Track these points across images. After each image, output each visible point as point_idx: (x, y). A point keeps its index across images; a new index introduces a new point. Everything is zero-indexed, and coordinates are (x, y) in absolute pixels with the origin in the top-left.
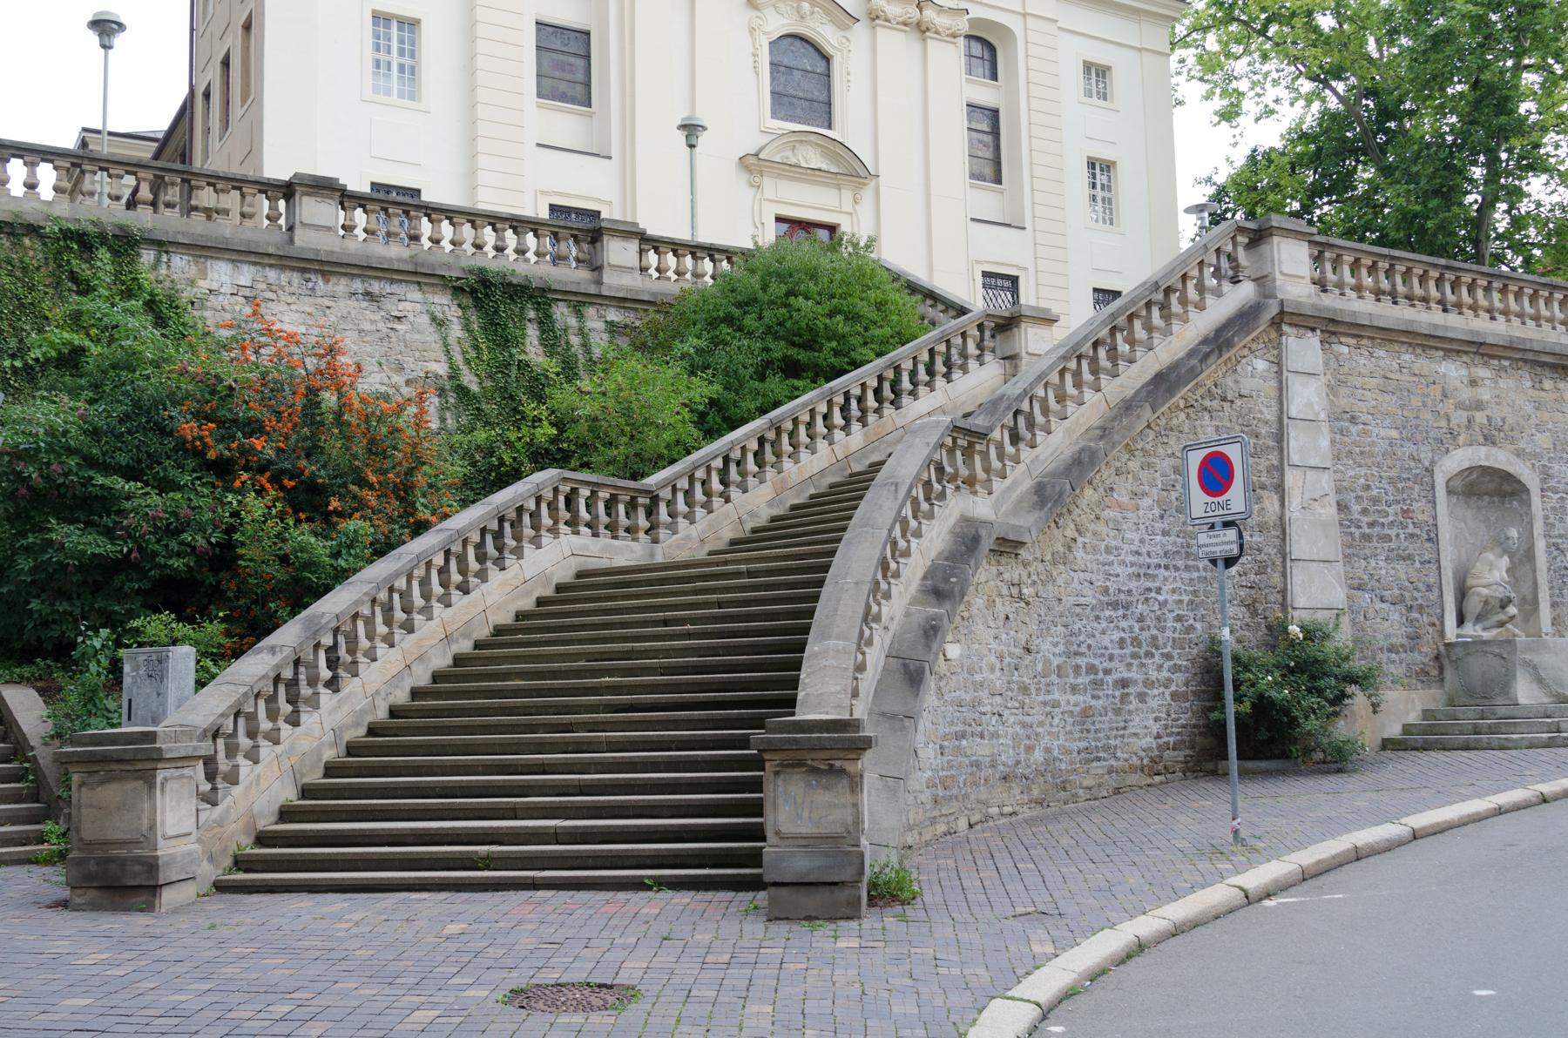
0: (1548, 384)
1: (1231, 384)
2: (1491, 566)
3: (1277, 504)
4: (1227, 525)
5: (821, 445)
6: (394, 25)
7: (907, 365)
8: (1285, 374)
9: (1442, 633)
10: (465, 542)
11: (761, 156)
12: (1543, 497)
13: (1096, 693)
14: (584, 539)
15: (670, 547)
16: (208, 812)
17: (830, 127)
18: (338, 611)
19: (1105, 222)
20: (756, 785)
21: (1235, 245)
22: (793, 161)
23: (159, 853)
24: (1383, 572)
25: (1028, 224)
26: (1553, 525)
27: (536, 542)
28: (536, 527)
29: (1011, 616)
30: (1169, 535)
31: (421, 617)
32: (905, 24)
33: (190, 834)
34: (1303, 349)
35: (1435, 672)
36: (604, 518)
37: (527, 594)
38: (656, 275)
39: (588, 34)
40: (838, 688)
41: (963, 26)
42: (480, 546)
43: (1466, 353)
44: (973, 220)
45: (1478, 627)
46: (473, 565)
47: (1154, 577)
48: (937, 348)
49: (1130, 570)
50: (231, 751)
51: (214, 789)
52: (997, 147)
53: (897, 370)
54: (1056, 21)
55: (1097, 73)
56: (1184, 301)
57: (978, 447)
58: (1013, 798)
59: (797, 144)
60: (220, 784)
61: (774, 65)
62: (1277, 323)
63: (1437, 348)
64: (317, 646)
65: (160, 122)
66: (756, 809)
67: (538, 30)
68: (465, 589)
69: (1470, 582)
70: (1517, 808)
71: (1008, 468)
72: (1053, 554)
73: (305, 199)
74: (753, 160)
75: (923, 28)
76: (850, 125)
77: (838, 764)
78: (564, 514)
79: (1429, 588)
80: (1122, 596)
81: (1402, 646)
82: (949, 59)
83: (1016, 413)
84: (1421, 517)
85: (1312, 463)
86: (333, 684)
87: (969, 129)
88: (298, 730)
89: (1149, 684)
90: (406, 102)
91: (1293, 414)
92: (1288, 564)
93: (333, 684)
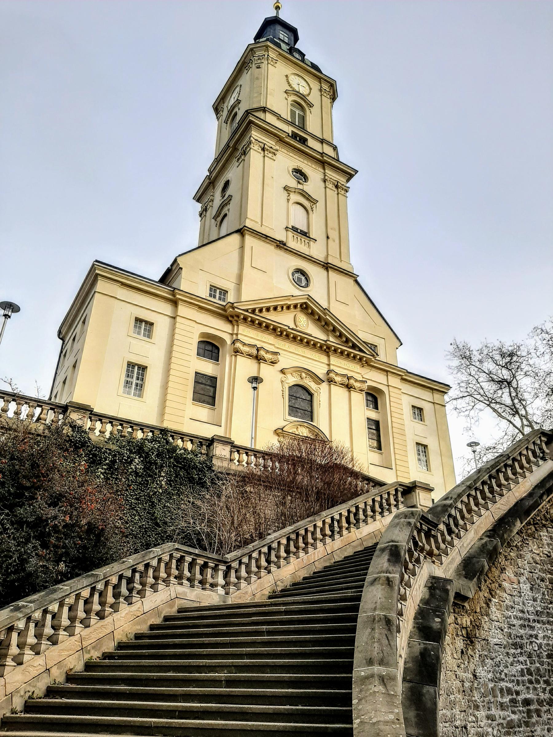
5: (319, 544)
6: (136, 368)
7: (362, 506)
13: (513, 709)
15: (235, 598)
17: (312, 421)
21: (541, 441)
22: (297, 433)
25: (394, 467)
30: (537, 601)
31: (65, 633)
36: (198, 576)
37: (145, 621)
38: (237, 463)
39: (216, 378)
40: (391, 717)
41: (365, 387)
42: (116, 587)
46: (110, 599)
47: (532, 628)
48: (376, 499)
49: (521, 622)
52: (379, 436)
53: (357, 508)
54: (401, 389)
59: (299, 426)
61: (290, 395)
67: (196, 375)
68: (101, 615)
71: (449, 549)
74: (280, 431)
78: (175, 572)
82: (359, 399)
87: (368, 428)
90: (136, 398)
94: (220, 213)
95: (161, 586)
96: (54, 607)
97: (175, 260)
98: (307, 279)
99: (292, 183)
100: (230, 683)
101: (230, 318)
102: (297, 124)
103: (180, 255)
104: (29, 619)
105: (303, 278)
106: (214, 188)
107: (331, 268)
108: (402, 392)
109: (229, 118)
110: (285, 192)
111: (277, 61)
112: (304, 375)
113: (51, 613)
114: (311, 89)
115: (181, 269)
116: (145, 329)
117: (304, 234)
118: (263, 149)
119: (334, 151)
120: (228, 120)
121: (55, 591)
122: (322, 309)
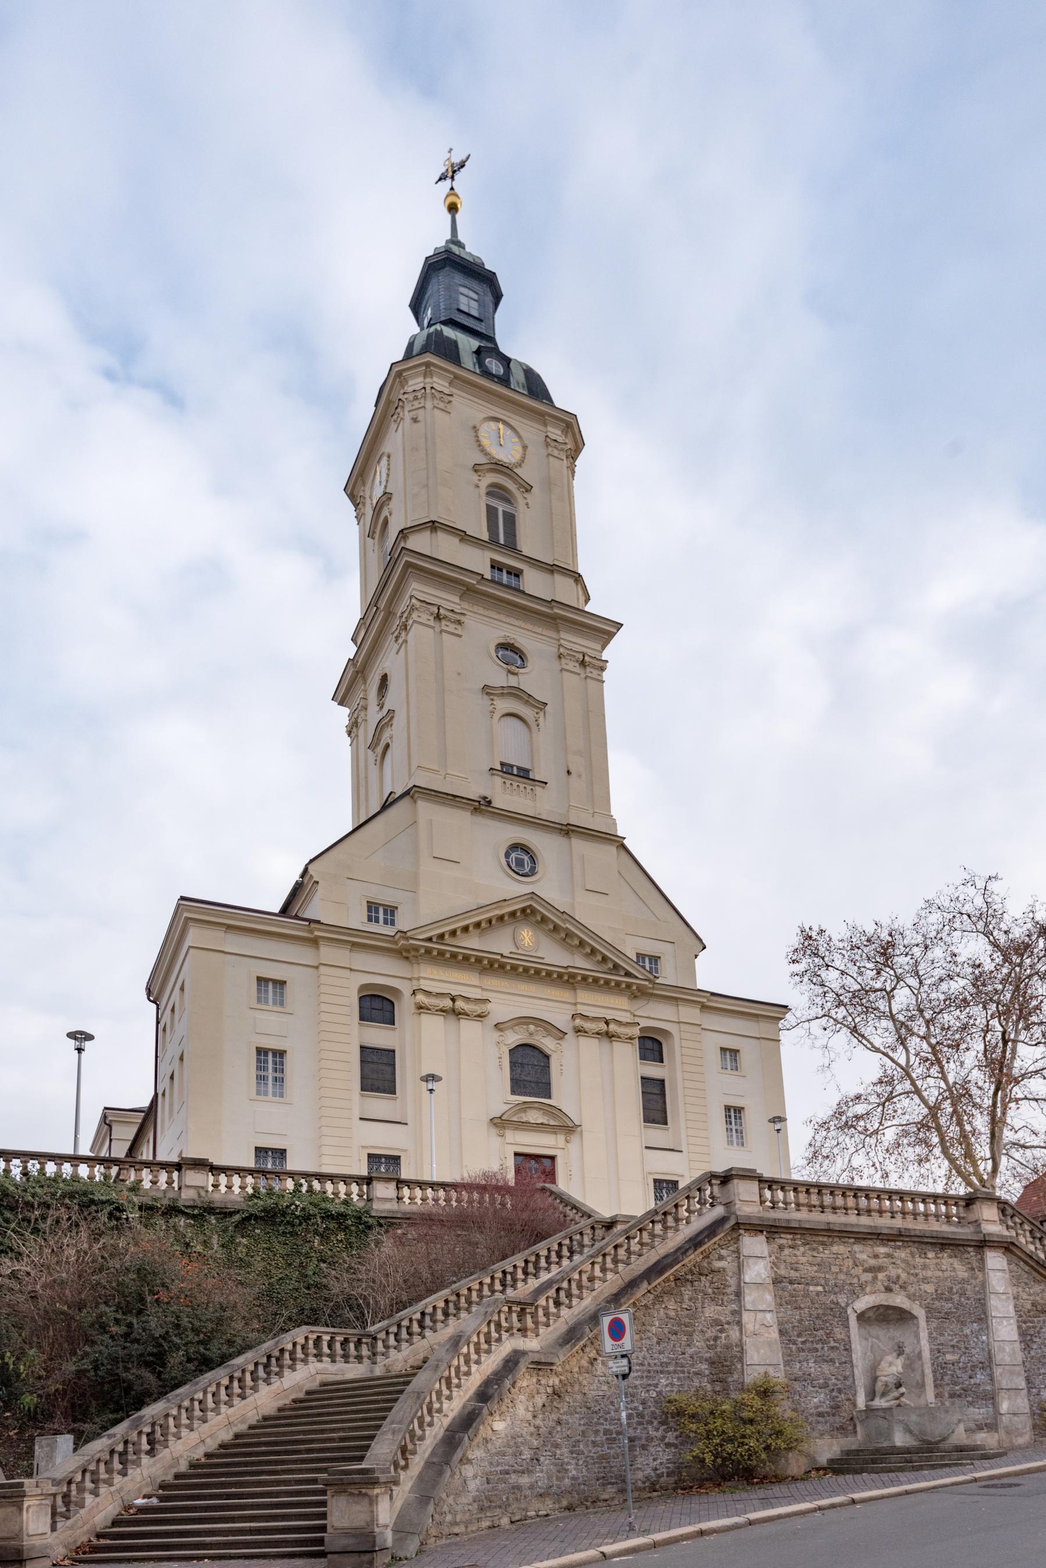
0: (931, 1255)
1: (706, 1265)
2: (891, 1364)
3: (738, 1334)
4: (623, 1356)
6: (270, 1055)
8: (742, 1258)
9: (855, 1405)
10: (243, 1371)
11: (503, 1118)
12: (927, 1321)
14: (326, 1364)
16: (63, 1523)
17: (550, 1097)
18: (153, 1413)
19: (738, 1144)
20: (323, 1504)
22: (524, 1119)
23: (24, 1543)
24: (813, 1370)
26: (936, 1338)
27: (293, 1368)
28: (293, 1359)
29: (547, 1404)
32: (598, 1034)
33: (46, 1534)
34: (754, 1245)
35: (851, 1428)
39: (394, 1051)
41: (636, 1032)
43: (871, 1239)
44: (647, 1148)
45: (883, 1400)
48: (564, 1242)
50: (81, 1489)
51: (68, 1510)
53: (538, 1256)
55: (731, 1054)
56: (677, 1220)
57: (528, 1311)
58: (547, 1506)
60: (72, 1508)
62: (737, 1226)
63: (849, 1238)
64: (140, 1433)
65: (145, 1102)
66: (323, 1516)
69: (878, 1373)
70: (841, 1505)
72: (579, 1368)
73: (188, 1172)
74: (499, 1121)
75: (610, 1035)
76: (562, 1095)
77: (364, 1491)
79: (846, 1378)
80: (630, 1390)
81: (827, 1413)
82: (627, 1055)
83: (558, 1290)
84: (839, 1336)
85: (761, 1308)
86: (151, 1453)
88: (126, 1478)
89: (650, 1439)
90: (277, 1099)
91: (747, 1280)
92: (745, 1367)
93: (151, 1453)
94: (379, 740)
95: (299, 1366)
96: (200, 1396)
97: (306, 870)
98: (533, 860)
99: (499, 678)
100: (342, 1439)
101: (404, 954)
102: (502, 541)
103: (311, 861)
104: (180, 1407)
105: (526, 858)
106: (365, 681)
107: (573, 831)
108: (702, 1029)
109: (375, 528)
110: (485, 696)
111: (450, 398)
112: (532, 1027)
113: (197, 1400)
114: (525, 448)
115: (317, 882)
116: (275, 993)
117: (524, 774)
118: (438, 617)
119: (577, 584)
120: (374, 532)
121: (197, 1383)
122: (558, 913)
